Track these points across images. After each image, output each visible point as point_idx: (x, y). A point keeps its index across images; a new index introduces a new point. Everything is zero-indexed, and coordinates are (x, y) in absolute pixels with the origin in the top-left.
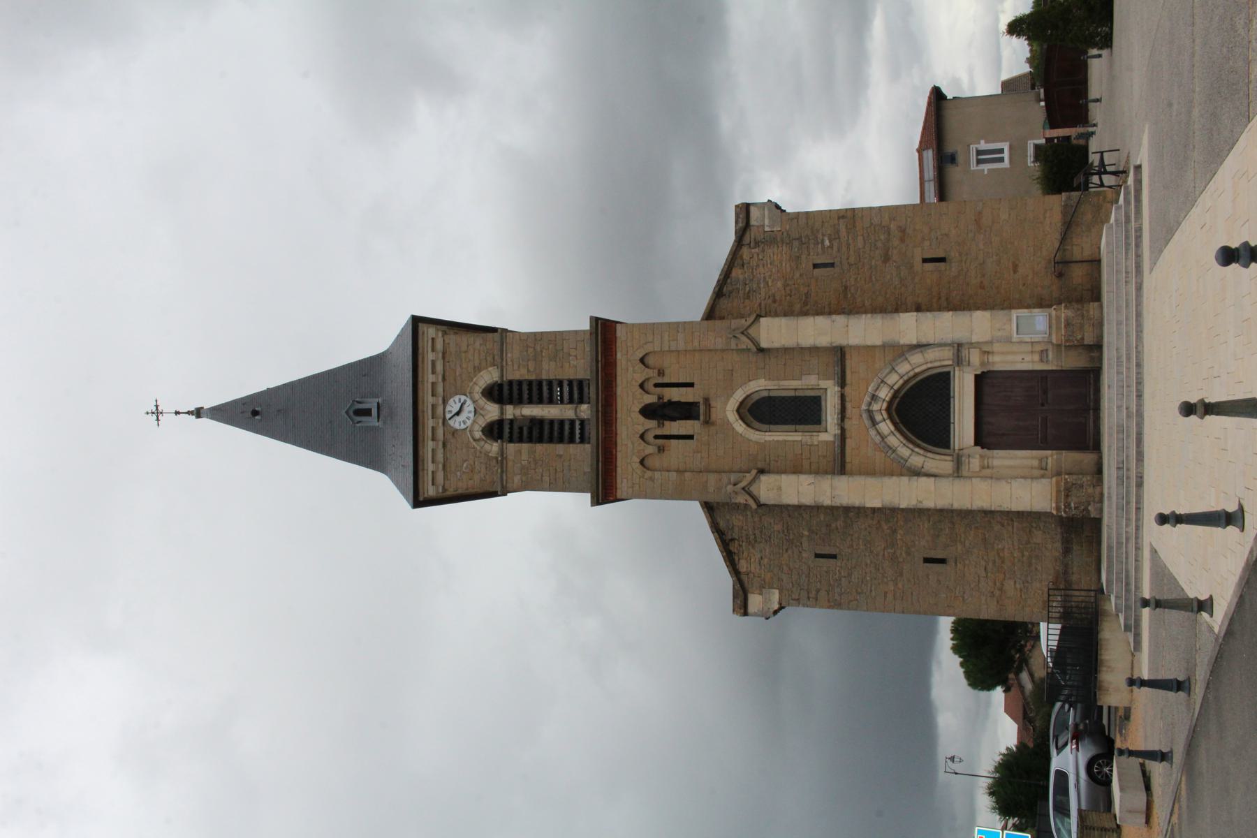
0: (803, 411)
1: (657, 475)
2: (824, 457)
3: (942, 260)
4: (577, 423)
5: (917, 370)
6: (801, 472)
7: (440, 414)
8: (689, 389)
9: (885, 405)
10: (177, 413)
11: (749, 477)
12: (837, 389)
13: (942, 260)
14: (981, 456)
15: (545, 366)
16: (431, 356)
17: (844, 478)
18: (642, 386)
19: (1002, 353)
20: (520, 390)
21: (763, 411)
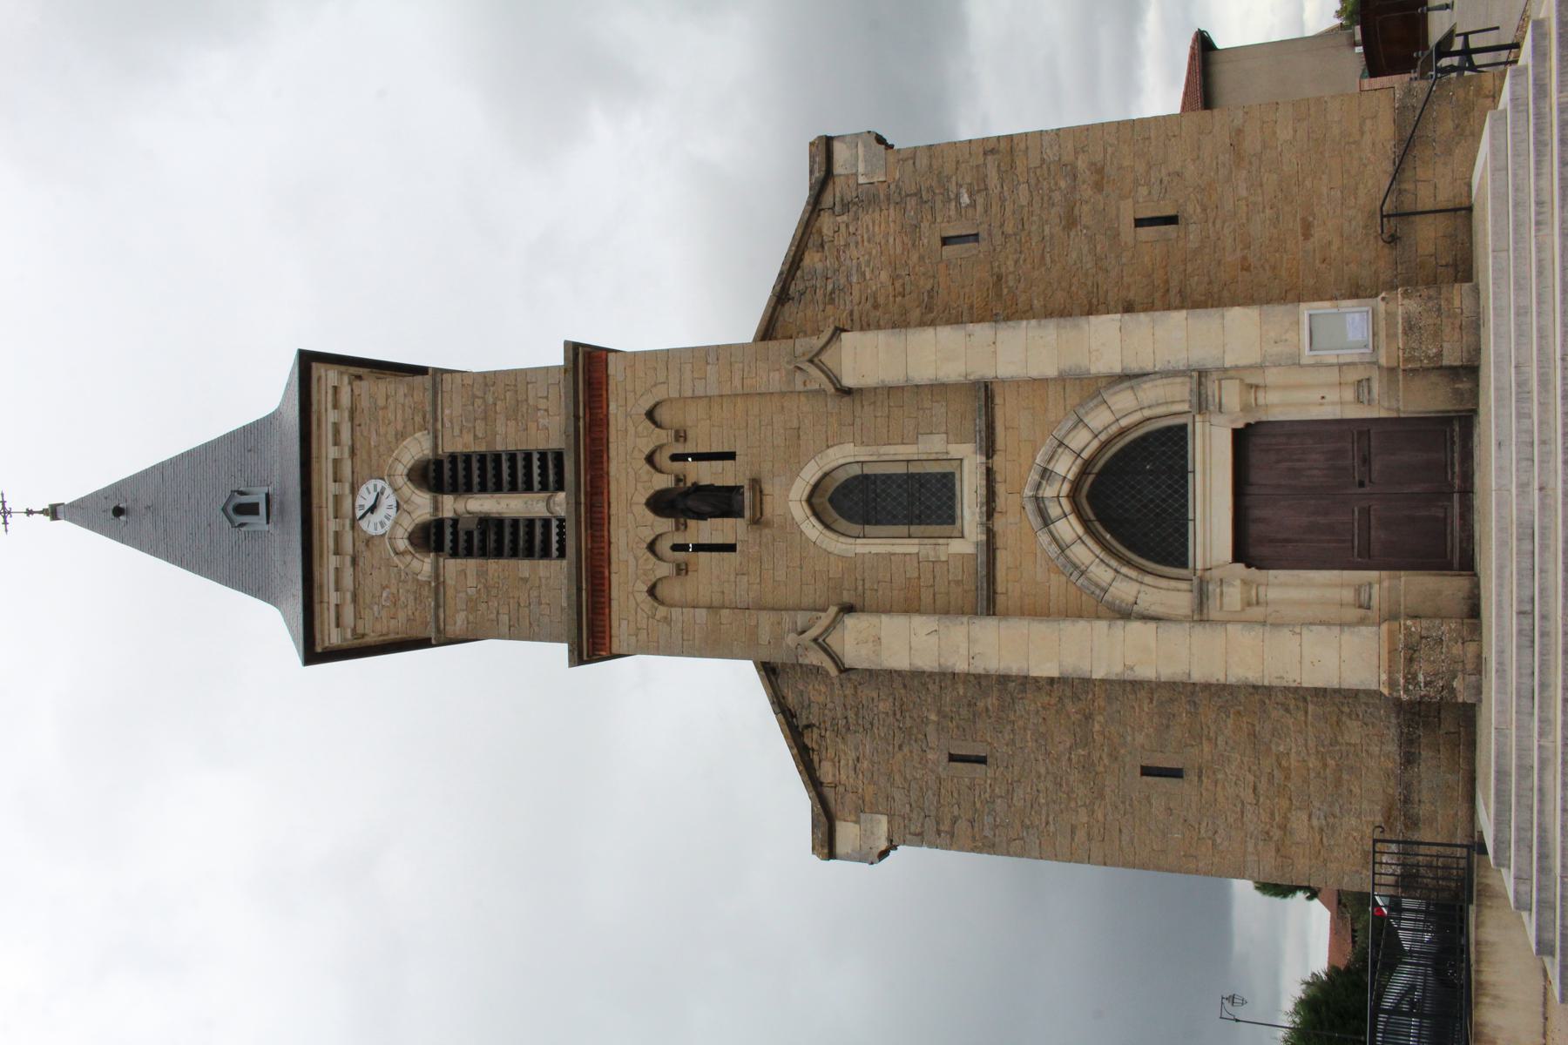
0: (920, 500)
1: (676, 612)
2: (958, 583)
3: (1171, 220)
4: (554, 523)
5: (1124, 423)
6: (918, 611)
7: (422, 508)
8: (728, 463)
9: (1066, 488)
10: (29, 512)
11: (825, 619)
12: (981, 459)
13: (1171, 220)
14: (1245, 582)
15: (500, 429)
16: (332, 416)
17: (991, 623)
18: (650, 459)
19: (1285, 387)
20: (468, 469)
21: (857, 501)
